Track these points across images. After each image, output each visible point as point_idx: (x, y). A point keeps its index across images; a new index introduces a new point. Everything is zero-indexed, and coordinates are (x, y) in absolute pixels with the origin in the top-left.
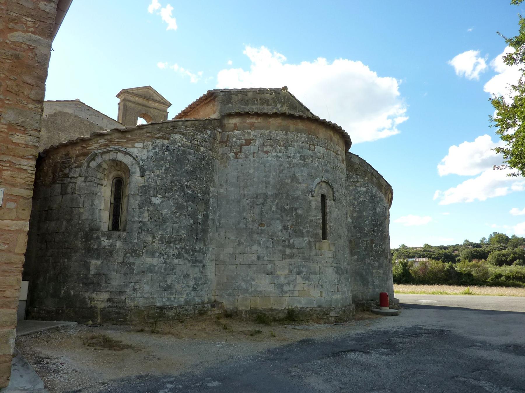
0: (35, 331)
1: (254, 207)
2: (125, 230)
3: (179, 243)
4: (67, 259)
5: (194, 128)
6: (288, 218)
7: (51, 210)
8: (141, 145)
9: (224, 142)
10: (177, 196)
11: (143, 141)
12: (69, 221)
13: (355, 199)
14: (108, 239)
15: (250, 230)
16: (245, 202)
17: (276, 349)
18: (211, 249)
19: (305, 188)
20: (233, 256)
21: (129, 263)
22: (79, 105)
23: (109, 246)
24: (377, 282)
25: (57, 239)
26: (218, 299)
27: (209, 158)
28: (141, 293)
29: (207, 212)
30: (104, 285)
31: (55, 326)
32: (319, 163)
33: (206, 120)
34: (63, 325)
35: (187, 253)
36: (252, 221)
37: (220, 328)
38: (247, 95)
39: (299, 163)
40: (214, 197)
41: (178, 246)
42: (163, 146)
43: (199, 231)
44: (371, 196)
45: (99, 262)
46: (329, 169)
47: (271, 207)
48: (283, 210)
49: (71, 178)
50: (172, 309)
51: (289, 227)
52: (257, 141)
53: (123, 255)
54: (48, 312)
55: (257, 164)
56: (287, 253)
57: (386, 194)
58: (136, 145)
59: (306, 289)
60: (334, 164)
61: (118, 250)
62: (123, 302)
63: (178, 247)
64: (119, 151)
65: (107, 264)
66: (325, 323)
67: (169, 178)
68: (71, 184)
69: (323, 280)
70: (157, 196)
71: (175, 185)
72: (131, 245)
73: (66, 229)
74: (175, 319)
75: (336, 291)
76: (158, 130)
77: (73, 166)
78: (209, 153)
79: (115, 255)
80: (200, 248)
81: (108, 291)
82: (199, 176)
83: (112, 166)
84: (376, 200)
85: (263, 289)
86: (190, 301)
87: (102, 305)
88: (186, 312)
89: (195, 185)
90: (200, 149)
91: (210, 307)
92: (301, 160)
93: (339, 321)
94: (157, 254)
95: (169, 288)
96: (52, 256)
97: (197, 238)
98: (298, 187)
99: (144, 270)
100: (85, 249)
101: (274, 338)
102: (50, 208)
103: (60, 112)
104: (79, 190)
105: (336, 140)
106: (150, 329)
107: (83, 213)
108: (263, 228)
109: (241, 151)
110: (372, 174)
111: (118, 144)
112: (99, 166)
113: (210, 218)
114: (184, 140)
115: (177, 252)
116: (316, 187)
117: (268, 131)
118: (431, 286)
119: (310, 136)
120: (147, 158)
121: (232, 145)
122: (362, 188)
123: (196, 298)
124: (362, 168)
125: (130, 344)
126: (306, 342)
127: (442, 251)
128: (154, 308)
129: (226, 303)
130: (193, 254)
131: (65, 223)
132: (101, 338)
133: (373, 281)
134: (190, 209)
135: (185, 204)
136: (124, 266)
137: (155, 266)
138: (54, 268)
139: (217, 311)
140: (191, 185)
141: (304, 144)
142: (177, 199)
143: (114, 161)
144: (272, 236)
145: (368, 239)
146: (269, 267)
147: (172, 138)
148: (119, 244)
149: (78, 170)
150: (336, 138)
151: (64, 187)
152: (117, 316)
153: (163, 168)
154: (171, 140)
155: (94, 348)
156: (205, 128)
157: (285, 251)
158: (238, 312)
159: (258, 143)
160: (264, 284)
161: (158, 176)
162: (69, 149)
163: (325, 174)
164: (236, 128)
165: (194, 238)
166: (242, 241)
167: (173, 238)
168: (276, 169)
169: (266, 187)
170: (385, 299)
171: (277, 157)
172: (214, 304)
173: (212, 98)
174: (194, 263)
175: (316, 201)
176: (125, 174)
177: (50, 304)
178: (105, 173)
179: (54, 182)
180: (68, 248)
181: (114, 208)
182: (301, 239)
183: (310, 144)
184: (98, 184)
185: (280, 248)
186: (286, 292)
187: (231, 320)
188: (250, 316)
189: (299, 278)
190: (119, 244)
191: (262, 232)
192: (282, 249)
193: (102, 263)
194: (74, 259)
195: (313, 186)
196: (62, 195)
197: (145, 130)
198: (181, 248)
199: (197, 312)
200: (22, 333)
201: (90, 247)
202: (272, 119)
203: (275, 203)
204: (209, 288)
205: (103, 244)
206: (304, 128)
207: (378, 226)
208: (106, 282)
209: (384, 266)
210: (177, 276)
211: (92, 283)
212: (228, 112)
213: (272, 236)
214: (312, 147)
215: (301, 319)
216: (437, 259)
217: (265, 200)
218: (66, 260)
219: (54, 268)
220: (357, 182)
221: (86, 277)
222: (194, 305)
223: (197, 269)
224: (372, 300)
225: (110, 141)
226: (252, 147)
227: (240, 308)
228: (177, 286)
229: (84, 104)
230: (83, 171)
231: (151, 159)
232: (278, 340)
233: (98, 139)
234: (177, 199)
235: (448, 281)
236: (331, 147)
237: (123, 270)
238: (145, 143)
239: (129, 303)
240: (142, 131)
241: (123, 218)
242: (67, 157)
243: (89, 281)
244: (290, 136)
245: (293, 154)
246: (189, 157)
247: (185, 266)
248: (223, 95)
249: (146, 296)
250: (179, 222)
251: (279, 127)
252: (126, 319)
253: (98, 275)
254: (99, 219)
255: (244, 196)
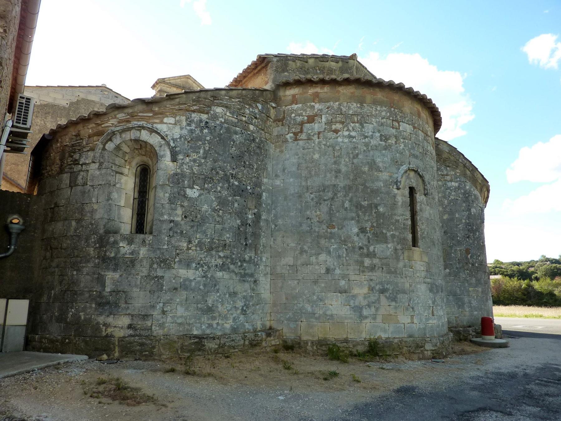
0: (25, 369)
1: (320, 204)
2: (151, 233)
3: (222, 251)
4: (77, 270)
5: (241, 100)
6: (366, 218)
7: (58, 206)
8: (172, 120)
9: (279, 121)
10: (219, 188)
11: (174, 115)
12: (79, 221)
13: (444, 197)
14: (128, 244)
15: (316, 234)
16: (308, 197)
17: (366, 405)
18: (264, 259)
19: (388, 178)
20: (294, 268)
21: (156, 277)
22: (106, 91)
23: (130, 254)
24: (474, 303)
25: (65, 245)
26: (275, 325)
27: (260, 140)
28: (172, 317)
29: (259, 210)
30: (123, 306)
31: (55, 363)
32: (405, 146)
33: (256, 90)
34: (66, 360)
35: (234, 264)
36: (318, 222)
37: (281, 366)
38: (307, 62)
39: (379, 144)
40: (268, 191)
41: (221, 254)
42: (201, 121)
43: (248, 235)
44: (464, 194)
45: (117, 275)
46: (418, 153)
47: (343, 203)
48: (359, 206)
49: (82, 165)
50: (214, 338)
51: (368, 229)
52: (323, 117)
53: (148, 266)
54: (52, 341)
55: (323, 146)
56: (366, 265)
57: (481, 191)
58: (165, 120)
59: (392, 312)
60: (423, 147)
61: (141, 260)
62: (148, 330)
63: (222, 255)
64: (143, 128)
65: (127, 278)
66: (420, 359)
67: (209, 164)
68: (82, 173)
69: (414, 301)
70: (193, 188)
71: (217, 173)
72: (158, 252)
73: (75, 230)
74: (218, 353)
75: (431, 315)
76: (194, 101)
77: (85, 150)
78: (261, 134)
79: (138, 266)
80: (251, 257)
81: (129, 314)
82: (247, 163)
83: (135, 148)
84: (470, 198)
85: (335, 312)
86: (238, 327)
87: (119, 334)
88: (233, 343)
89: (243, 174)
90: (248, 128)
91: (264, 337)
92: (381, 140)
93: (437, 356)
94: (194, 265)
95: (210, 310)
96: (58, 266)
97: (246, 245)
98: (378, 177)
99: (176, 286)
100: (98, 257)
101: (358, 385)
102: (57, 205)
103: (83, 99)
104: (92, 180)
105: (425, 116)
106: (183, 368)
107: (96, 210)
108: (333, 231)
109: (301, 131)
110: (465, 166)
111: (142, 118)
112: (118, 148)
113: (263, 217)
114: (228, 114)
115: (220, 262)
116: (402, 177)
117: (337, 103)
118: (507, 307)
119: (393, 109)
120: (180, 138)
121: (290, 123)
122: (453, 183)
123: (246, 324)
124: (452, 158)
125: (151, 395)
126: (405, 392)
127: (515, 268)
128: (190, 338)
129: (284, 330)
130: (241, 266)
131: (74, 223)
132: (113, 382)
133: (470, 302)
134: (236, 205)
135: (230, 198)
136: (151, 280)
137: (191, 281)
138: (61, 283)
139: (274, 341)
140: (237, 173)
141: (385, 120)
142: (220, 192)
143: (137, 141)
144: (345, 241)
145: (463, 248)
146: (343, 283)
147: (212, 112)
148: (143, 252)
149: (91, 154)
150: (425, 114)
151: (74, 177)
152: (140, 348)
153: (202, 151)
154: (211, 115)
155: (98, 400)
156: (255, 100)
157: (363, 262)
158: (302, 344)
159: (324, 119)
160: (336, 306)
161: (194, 161)
162: (80, 127)
163: (413, 160)
164: (294, 101)
165: (242, 244)
166: (306, 248)
167: (215, 243)
168: (348, 153)
169: (336, 177)
170: (487, 326)
171: (350, 137)
172: (270, 332)
173: (263, 65)
174: (243, 277)
175: (403, 195)
176: (152, 160)
177: (55, 331)
178: (126, 158)
179: (61, 171)
180: (77, 256)
181: (139, 205)
182: (384, 246)
183: (393, 120)
184: (117, 172)
185: (356, 257)
186: (366, 317)
187: (293, 355)
188: (318, 349)
189: (382, 298)
190: (143, 252)
191: (332, 236)
192: (360, 259)
193: (121, 276)
194: (85, 271)
195: (399, 174)
196: (71, 187)
197: (177, 100)
198: (226, 257)
199: (247, 343)
200: (6, 374)
201: (105, 255)
202: (343, 87)
203: (348, 198)
204: (263, 310)
205: (123, 251)
206: (385, 99)
207: (474, 232)
208: (126, 303)
209: (483, 282)
210: (220, 295)
211: (108, 303)
212: (284, 80)
213: (345, 242)
214: (396, 124)
215: (388, 353)
216: (511, 276)
217: (336, 194)
218: (75, 273)
219: (61, 283)
220: (447, 175)
221: (100, 295)
222: (244, 333)
223: (247, 285)
224: (470, 327)
225: (132, 116)
226: (316, 125)
227: (305, 338)
228: (220, 308)
229: (112, 90)
230: (97, 155)
231: (185, 139)
232: (364, 388)
233: (116, 112)
234: (220, 192)
235: (526, 301)
236: (419, 125)
237: (148, 286)
238: (177, 118)
239: (157, 331)
240: (173, 102)
241: (149, 217)
242: (78, 138)
243: (104, 301)
244: (367, 109)
245: (371, 133)
246: (235, 137)
247: (232, 282)
248: (278, 61)
249: (180, 321)
250: (223, 223)
251: (352, 98)
252: (152, 353)
253: (116, 292)
254: (119, 218)
255: (307, 188)
